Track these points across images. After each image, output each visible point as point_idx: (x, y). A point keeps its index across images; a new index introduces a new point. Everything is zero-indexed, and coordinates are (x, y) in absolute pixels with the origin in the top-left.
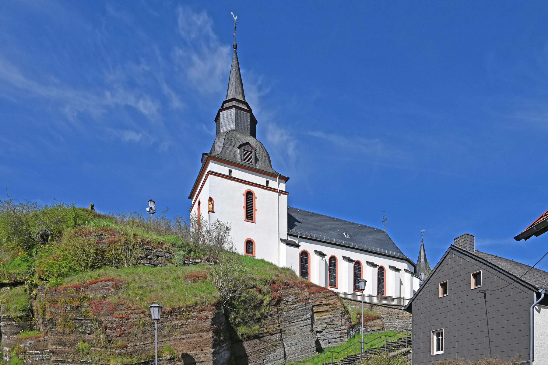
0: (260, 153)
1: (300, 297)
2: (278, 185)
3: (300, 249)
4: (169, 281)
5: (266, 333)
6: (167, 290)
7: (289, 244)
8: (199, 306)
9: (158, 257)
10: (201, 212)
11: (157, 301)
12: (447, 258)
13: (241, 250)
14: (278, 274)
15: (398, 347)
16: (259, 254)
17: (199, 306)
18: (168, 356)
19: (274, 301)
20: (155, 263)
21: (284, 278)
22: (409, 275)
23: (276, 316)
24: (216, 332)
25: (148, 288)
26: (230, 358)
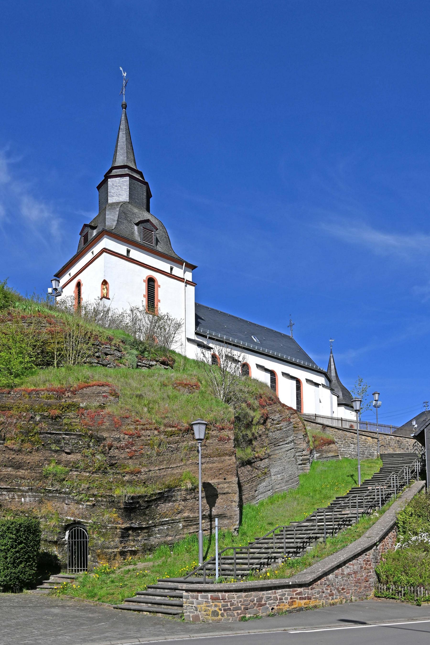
2: (184, 273)
5: (256, 458)
20: (104, 362)
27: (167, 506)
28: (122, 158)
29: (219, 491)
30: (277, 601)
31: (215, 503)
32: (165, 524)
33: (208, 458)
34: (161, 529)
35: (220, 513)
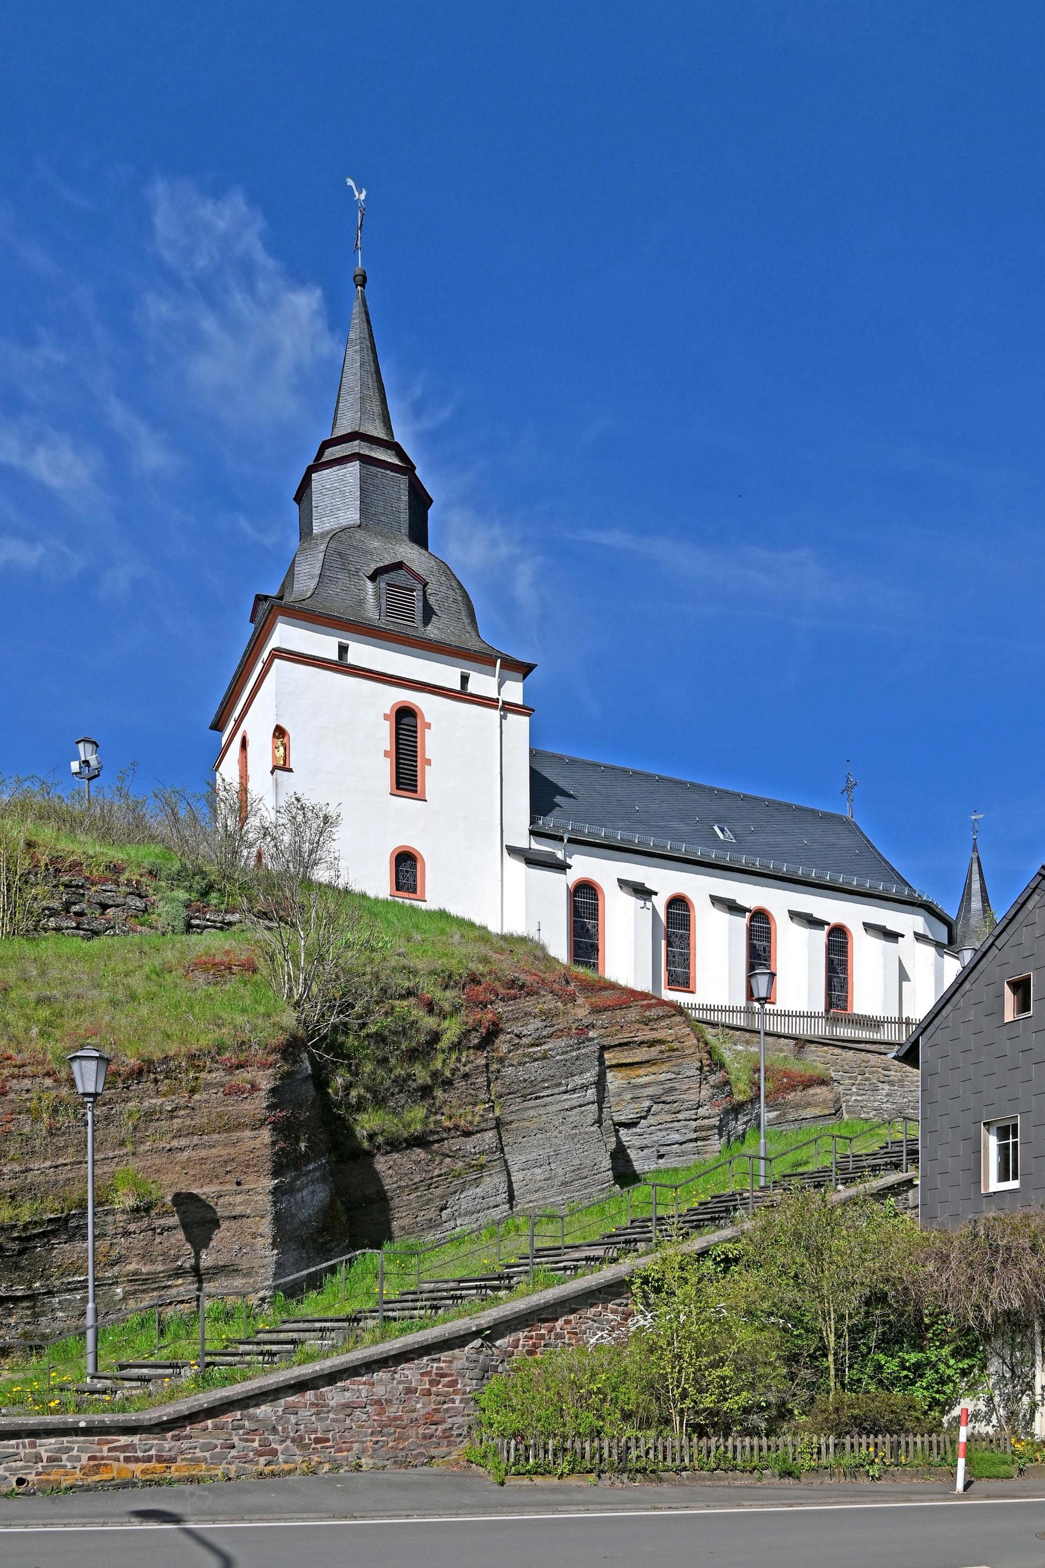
0: (438, 592)
1: (561, 1023)
2: (500, 686)
3: (573, 876)
4: (136, 981)
6: (129, 1008)
7: (532, 860)
8: (228, 1055)
9: (104, 907)
10: (249, 772)
11: (95, 1040)
12: (1030, 905)
13: (376, 882)
14: (490, 953)
15: (874, 1168)
16: (437, 892)
17: (228, 1055)
18: (131, 1202)
19: (474, 1034)
20: (95, 925)
21: (507, 966)
22: (931, 950)
23: (481, 1080)
24: (285, 1130)
25: (69, 1003)
26: (333, 1202)
27: (78, 1249)
28: (349, 414)
29: (220, 1212)
30: (40, 1464)
31: (211, 1239)
32: (76, 1289)
33: (196, 1137)
34: (66, 1300)
35: (221, 1263)
